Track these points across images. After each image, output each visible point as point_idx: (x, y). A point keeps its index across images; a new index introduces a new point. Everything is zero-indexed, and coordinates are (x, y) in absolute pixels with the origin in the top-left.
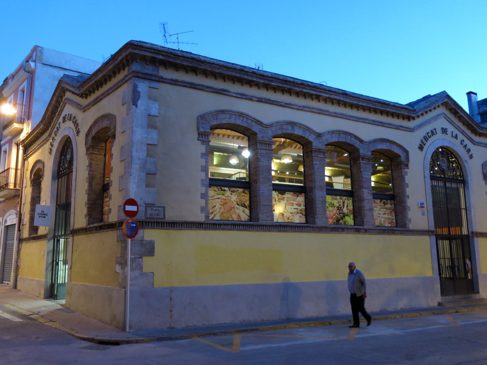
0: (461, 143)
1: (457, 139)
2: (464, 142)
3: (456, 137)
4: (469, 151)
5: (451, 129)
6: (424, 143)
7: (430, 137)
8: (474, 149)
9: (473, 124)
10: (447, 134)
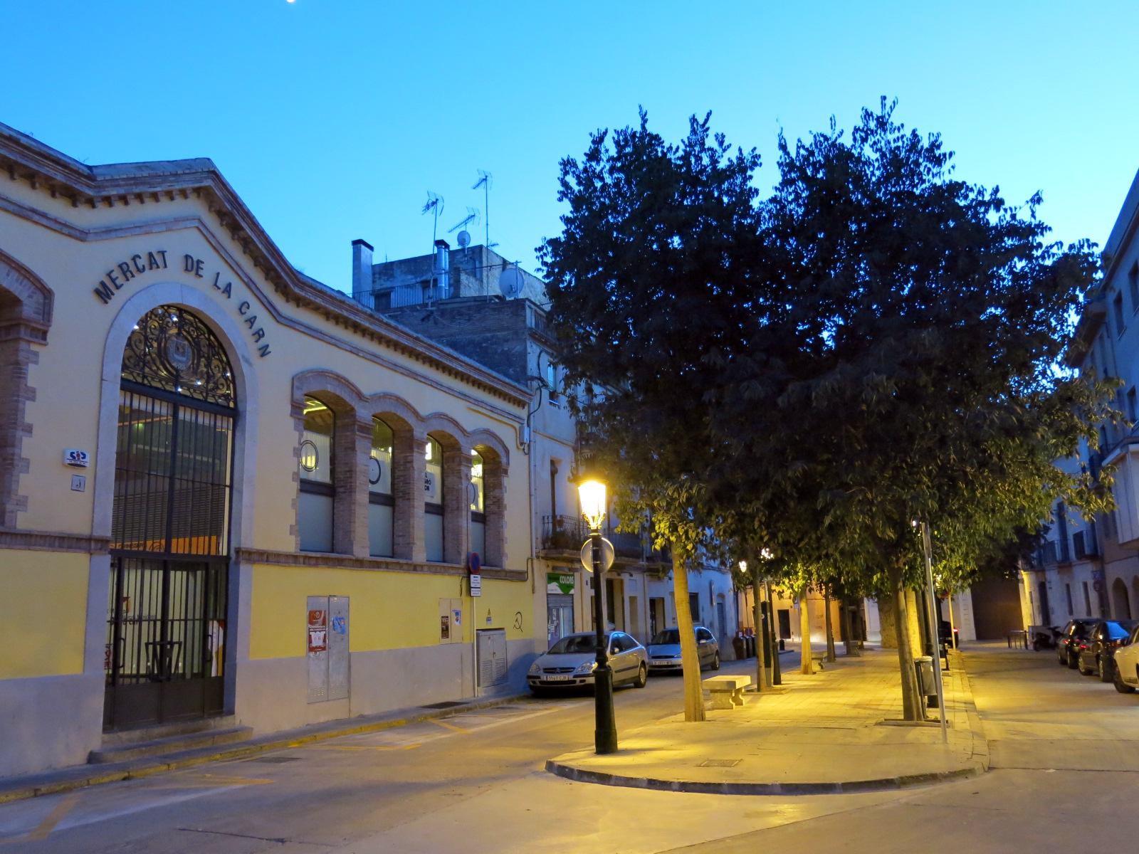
0: (240, 309)
1: (229, 297)
3: (228, 290)
4: (260, 334)
5: (213, 262)
7: (141, 270)
9: (279, 269)
10: (201, 276)
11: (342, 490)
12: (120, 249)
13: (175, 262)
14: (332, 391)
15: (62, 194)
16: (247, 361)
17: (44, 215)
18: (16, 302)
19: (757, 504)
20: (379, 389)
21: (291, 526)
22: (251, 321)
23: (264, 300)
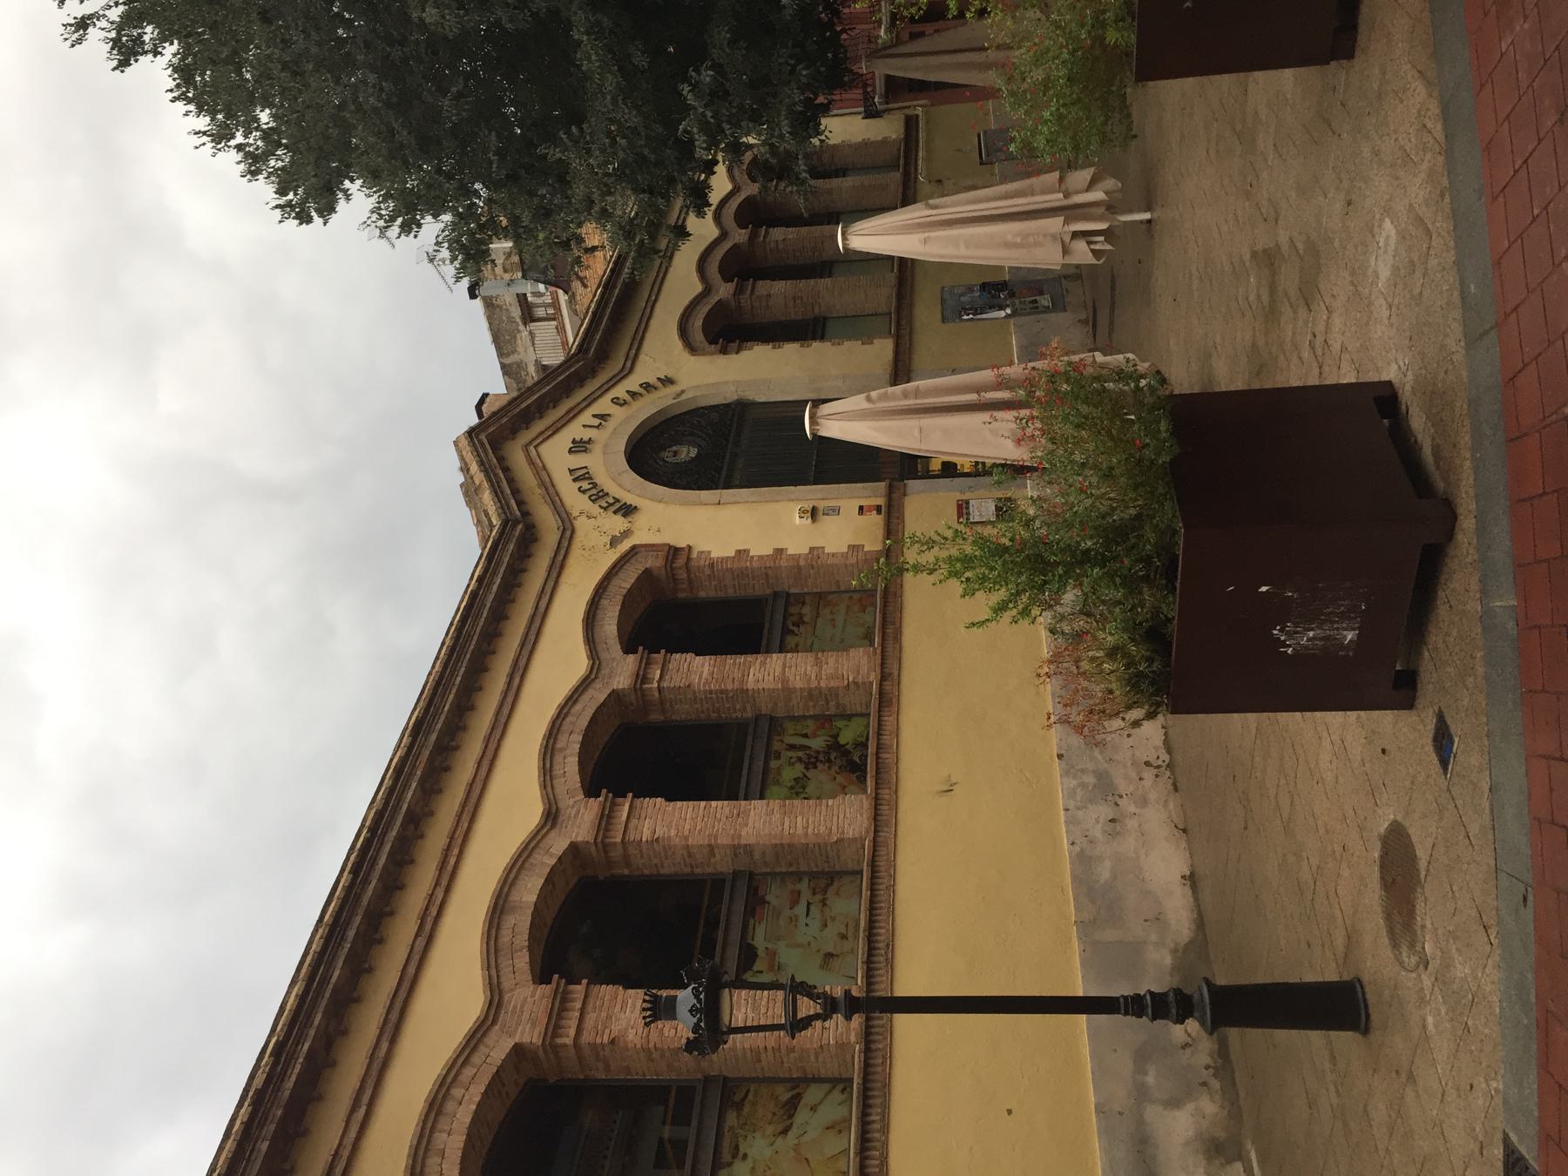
0: (621, 405)
1: (609, 415)
2: (618, 398)
3: (603, 417)
4: (647, 387)
5: (575, 430)
6: (611, 501)
7: (595, 485)
8: (647, 370)
11: (816, 310)
12: (575, 501)
13: (579, 461)
14: (526, 953)
15: (509, 594)
16: (679, 395)
17: (447, 851)
18: (647, 572)
19: (679, 203)
20: (694, 276)
21: (823, 548)
22: (633, 394)
23: (606, 387)
